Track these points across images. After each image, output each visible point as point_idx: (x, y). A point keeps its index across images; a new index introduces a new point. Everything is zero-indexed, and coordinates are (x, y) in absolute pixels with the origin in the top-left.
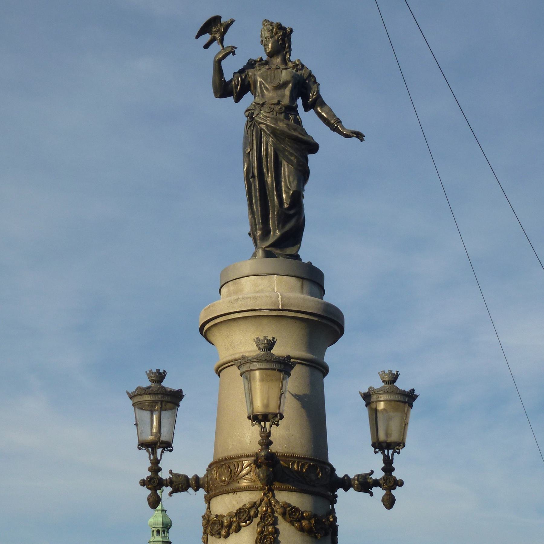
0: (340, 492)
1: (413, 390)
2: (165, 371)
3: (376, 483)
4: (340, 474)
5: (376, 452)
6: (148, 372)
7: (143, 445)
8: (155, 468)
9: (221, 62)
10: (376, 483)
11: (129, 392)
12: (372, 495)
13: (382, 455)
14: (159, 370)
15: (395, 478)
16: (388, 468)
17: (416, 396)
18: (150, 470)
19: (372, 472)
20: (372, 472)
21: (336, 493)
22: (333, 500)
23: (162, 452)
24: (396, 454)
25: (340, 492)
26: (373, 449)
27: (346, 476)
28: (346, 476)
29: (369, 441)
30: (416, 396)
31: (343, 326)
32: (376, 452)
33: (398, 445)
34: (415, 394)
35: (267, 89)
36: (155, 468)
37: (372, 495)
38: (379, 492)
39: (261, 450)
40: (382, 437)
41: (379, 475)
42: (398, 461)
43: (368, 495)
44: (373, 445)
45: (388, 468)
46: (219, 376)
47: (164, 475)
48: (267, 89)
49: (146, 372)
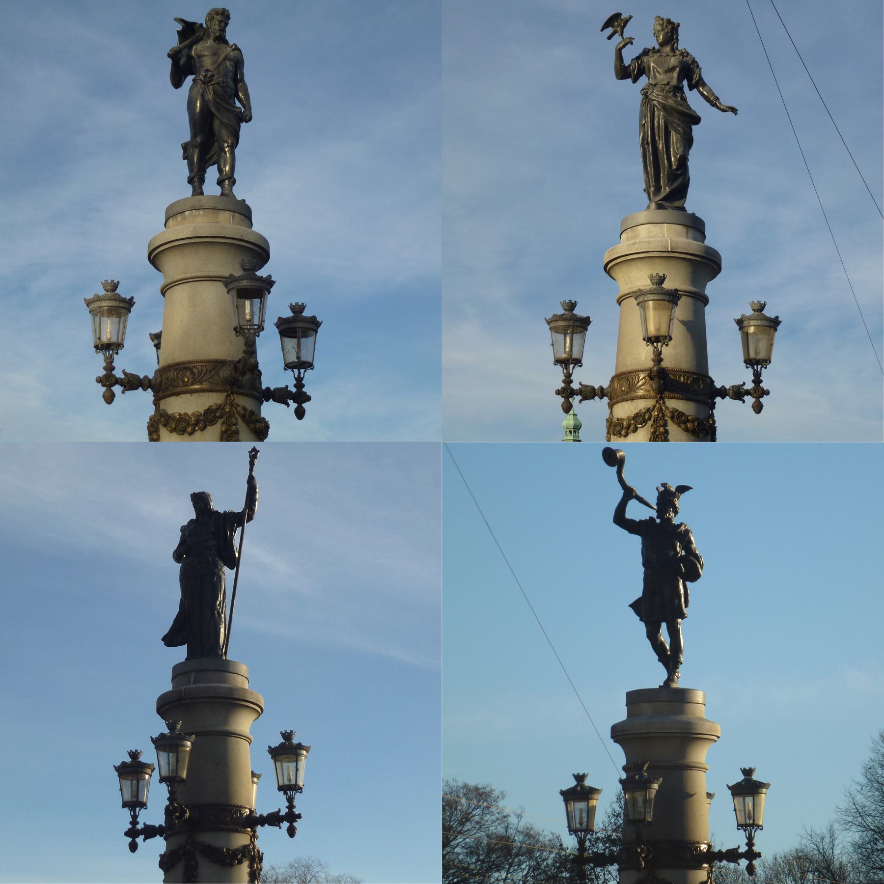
0: (718, 400)
3: (748, 393)
5: (747, 367)
7: (558, 361)
8: (738, 393)
10: (748, 393)
12: (744, 402)
16: (757, 380)
17: (274, 282)
22: (712, 406)
23: (305, 371)
24: (763, 369)
25: (718, 400)
26: (745, 364)
27: (723, 386)
28: (723, 386)
30: (274, 282)
32: (747, 367)
33: (765, 362)
34: (272, 280)
36: (738, 393)
37: (744, 402)
38: (750, 400)
40: (752, 355)
41: (749, 386)
42: (765, 374)
43: (741, 402)
44: (745, 362)
45: (757, 380)
47: (293, 405)
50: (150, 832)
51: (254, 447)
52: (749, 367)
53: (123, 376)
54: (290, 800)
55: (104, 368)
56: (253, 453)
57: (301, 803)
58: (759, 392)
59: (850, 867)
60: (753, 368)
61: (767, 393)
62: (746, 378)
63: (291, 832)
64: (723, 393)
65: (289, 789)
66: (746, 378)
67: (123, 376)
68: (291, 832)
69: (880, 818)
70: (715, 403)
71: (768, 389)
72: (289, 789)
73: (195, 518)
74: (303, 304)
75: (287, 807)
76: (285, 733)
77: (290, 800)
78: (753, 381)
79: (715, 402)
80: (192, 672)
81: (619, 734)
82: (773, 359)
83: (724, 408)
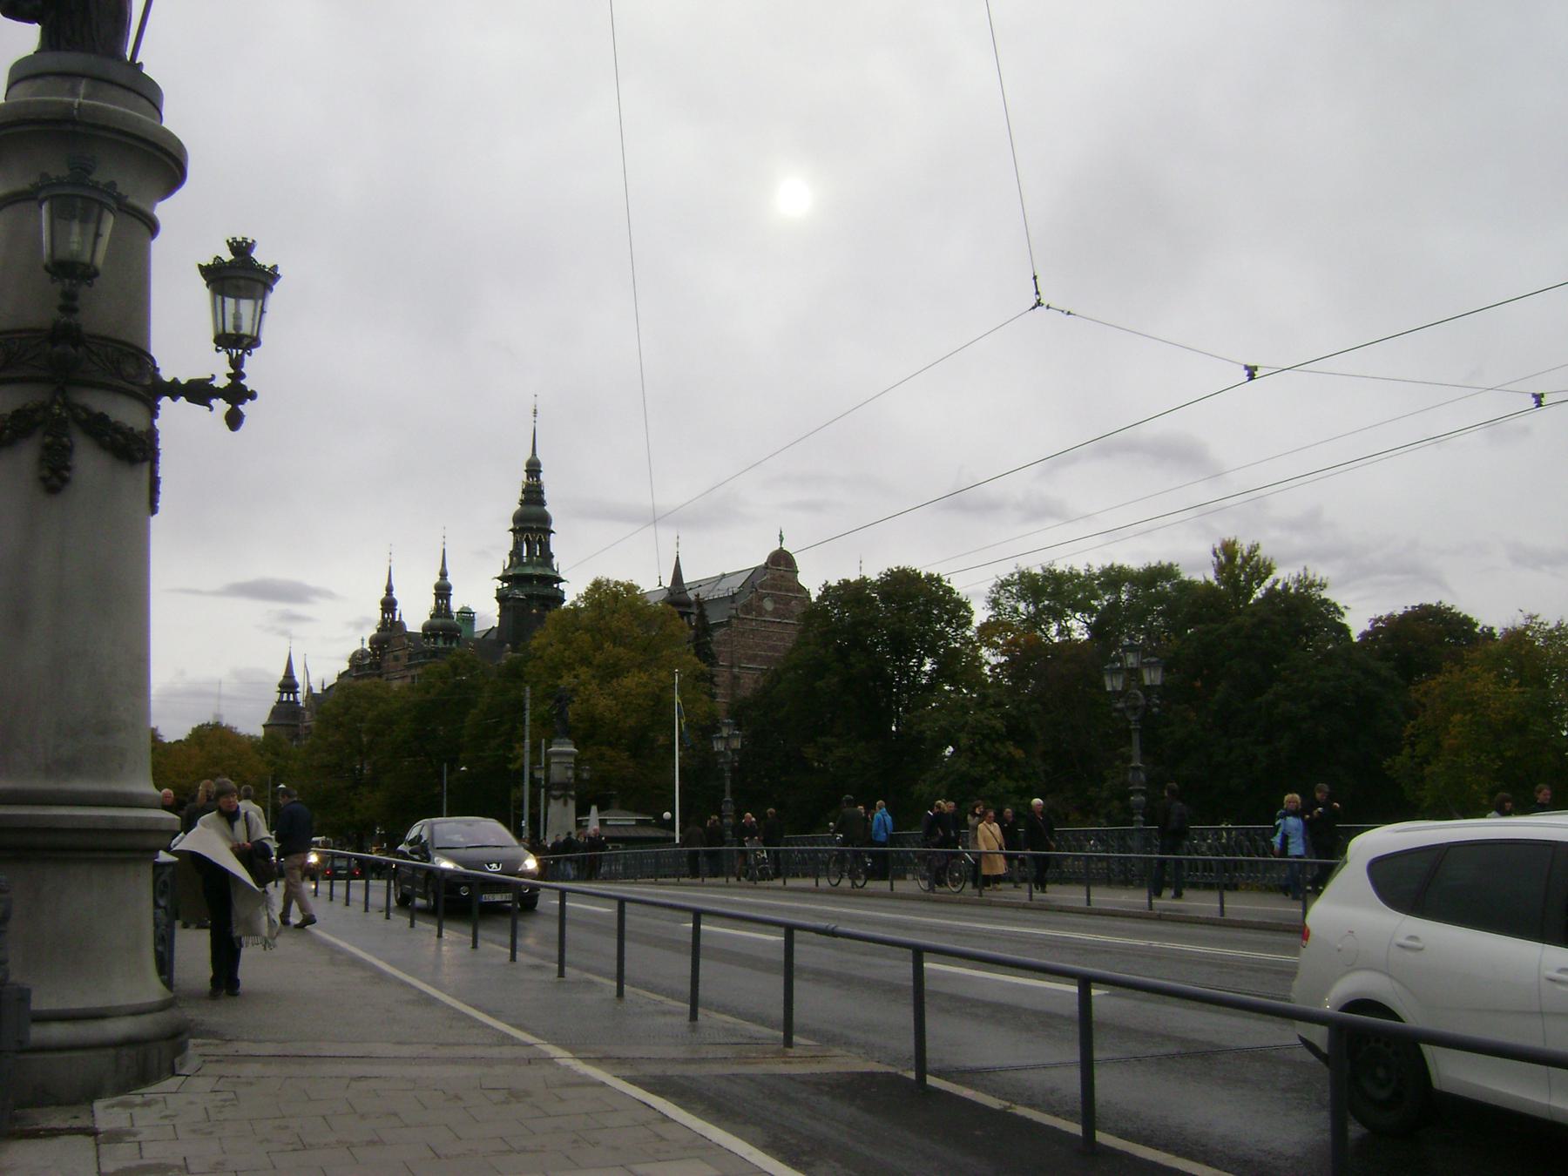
0: (165, 402)
1: (275, 267)
2: (253, 241)
3: (218, 393)
4: (166, 375)
6: (231, 241)
8: (199, 392)
10: (218, 393)
11: (228, 410)
12: (211, 409)
15: (244, 387)
16: (237, 375)
19: (213, 377)
20: (213, 377)
22: (154, 412)
25: (165, 402)
26: (215, 345)
27: (175, 379)
28: (175, 379)
36: (199, 392)
37: (211, 409)
38: (221, 406)
39: (558, 586)
42: (250, 364)
43: (208, 409)
45: (237, 375)
46: (1247, 368)
49: (228, 241)
54: (237, 363)
57: (255, 369)
58: (237, 393)
63: (234, 420)
64: (175, 390)
65: (236, 342)
66: (216, 368)
68: (234, 420)
71: (254, 389)
72: (236, 342)
75: (229, 376)
76: (241, 243)
77: (237, 363)
79: (159, 406)
80: (83, 76)
81: (526, 471)
82: (264, 338)
83: (174, 417)
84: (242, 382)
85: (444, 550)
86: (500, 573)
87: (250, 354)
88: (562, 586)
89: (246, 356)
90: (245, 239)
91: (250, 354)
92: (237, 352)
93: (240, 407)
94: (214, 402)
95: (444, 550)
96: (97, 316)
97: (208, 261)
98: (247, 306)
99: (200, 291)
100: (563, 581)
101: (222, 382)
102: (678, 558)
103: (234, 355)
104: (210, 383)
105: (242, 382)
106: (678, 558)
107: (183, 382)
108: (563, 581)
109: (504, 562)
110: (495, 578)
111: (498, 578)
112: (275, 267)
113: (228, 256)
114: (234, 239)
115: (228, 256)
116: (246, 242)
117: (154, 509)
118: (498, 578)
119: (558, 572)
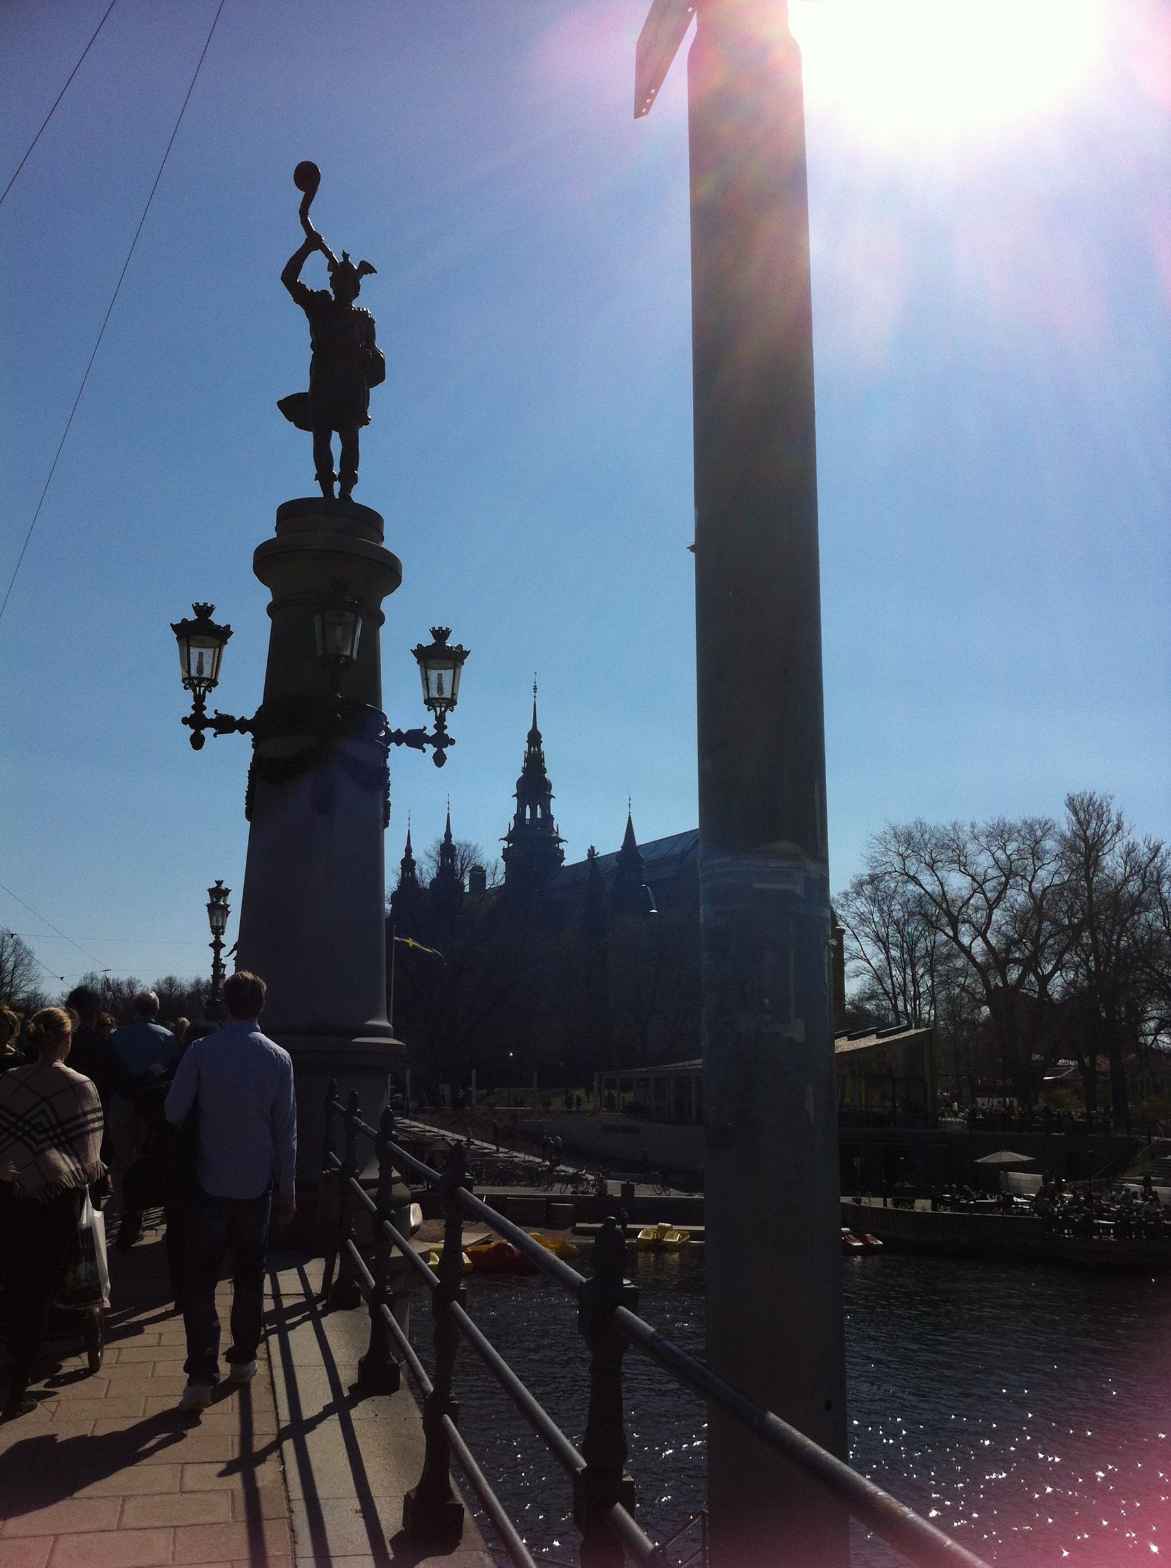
1: (228, 626)
5: (429, 710)
8: (415, 739)
9: (311, 252)
12: (216, 712)
13: (180, 622)
14: (207, 604)
16: (440, 724)
18: (193, 707)
21: (194, 712)
24: (448, 712)
29: (420, 696)
31: (399, 572)
32: (429, 710)
33: (451, 703)
35: (981, 1409)
36: (415, 739)
37: (424, 751)
38: (209, 714)
40: (434, 694)
41: (431, 732)
44: (426, 702)
45: (440, 724)
47: (431, 749)
48: (981, 1409)
49: (193, 605)
50: (225, 724)
51: (225, 946)
52: (188, 689)
53: (425, 746)
55: (193, 707)
56: (1112, 1232)
58: (442, 740)
59: (529, 1345)
60: (194, 691)
61: (185, 721)
62: (426, 721)
63: (439, 760)
66: (426, 721)
67: (425, 746)
68: (439, 760)
69: (886, 1404)
70: (202, 735)
72: (442, 703)
73: (277, 1335)
74: (447, 629)
78: (435, 727)
82: (460, 699)
83: (399, 758)
84: (445, 732)
85: (448, 814)
86: (505, 834)
87: (210, 692)
88: (561, 846)
89: (207, 692)
90: (440, 628)
91: (210, 692)
92: (441, 710)
93: (444, 749)
94: (214, 716)
95: (448, 814)
96: (454, 698)
97: (314, 477)
98: (447, 675)
99: (414, 668)
100: (562, 841)
101: (431, 732)
102: (630, 818)
103: (438, 713)
104: (424, 732)
105: (445, 732)
106: (630, 818)
107: (404, 732)
108: (562, 841)
109: (510, 824)
110: (502, 839)
111: (504, 839)
112: (228, 626)
113: (192, 616)
114: (197, 604)
115: (192, 616)
116: (442, 630)
117: (386, 825)
118: (504, 839)
119: (557, 833)
